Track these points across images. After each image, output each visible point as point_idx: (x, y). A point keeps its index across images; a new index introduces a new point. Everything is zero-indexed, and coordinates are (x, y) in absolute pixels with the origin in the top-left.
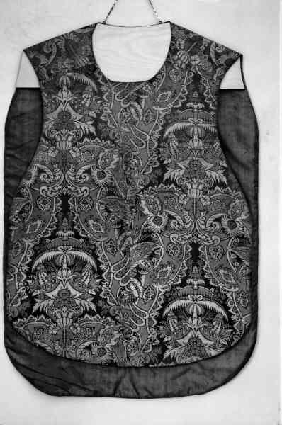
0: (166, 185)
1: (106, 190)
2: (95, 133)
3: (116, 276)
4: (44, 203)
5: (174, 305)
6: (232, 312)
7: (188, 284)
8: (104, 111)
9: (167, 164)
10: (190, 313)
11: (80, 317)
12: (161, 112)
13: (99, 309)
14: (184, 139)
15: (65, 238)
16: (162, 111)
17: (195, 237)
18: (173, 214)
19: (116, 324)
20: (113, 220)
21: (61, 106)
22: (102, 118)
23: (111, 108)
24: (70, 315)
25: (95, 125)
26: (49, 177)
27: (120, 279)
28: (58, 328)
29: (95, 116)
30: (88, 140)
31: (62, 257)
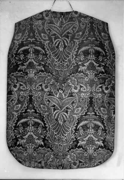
0: (78, 148)
1: (48, 93)
2: (43, 145)
3: (53, 56)
4: (22, 98)
5: (81, 124)
6: (107, 51)
7: (88, 115)
8: (47, 135)
9: (78, 140)
10: (89, 127)
11: (37, 148)
12: (77, 42)
13: (45, 145)
14: (86, 129)
15: (31, 41)
16: (78, 42)
17: (91, 95)
18: (82, 85)
19: (52, 151)
20: (51, 105)
21: (30, 60)
22: (47, 64)
23: (51, 61)
24: (33, 147)
25: (43, 141)
26: (24, 88)
27: (54, 131)
28: (27, 153)
29: (43, 137)
30: (41, 148)
31: (29, 121)
